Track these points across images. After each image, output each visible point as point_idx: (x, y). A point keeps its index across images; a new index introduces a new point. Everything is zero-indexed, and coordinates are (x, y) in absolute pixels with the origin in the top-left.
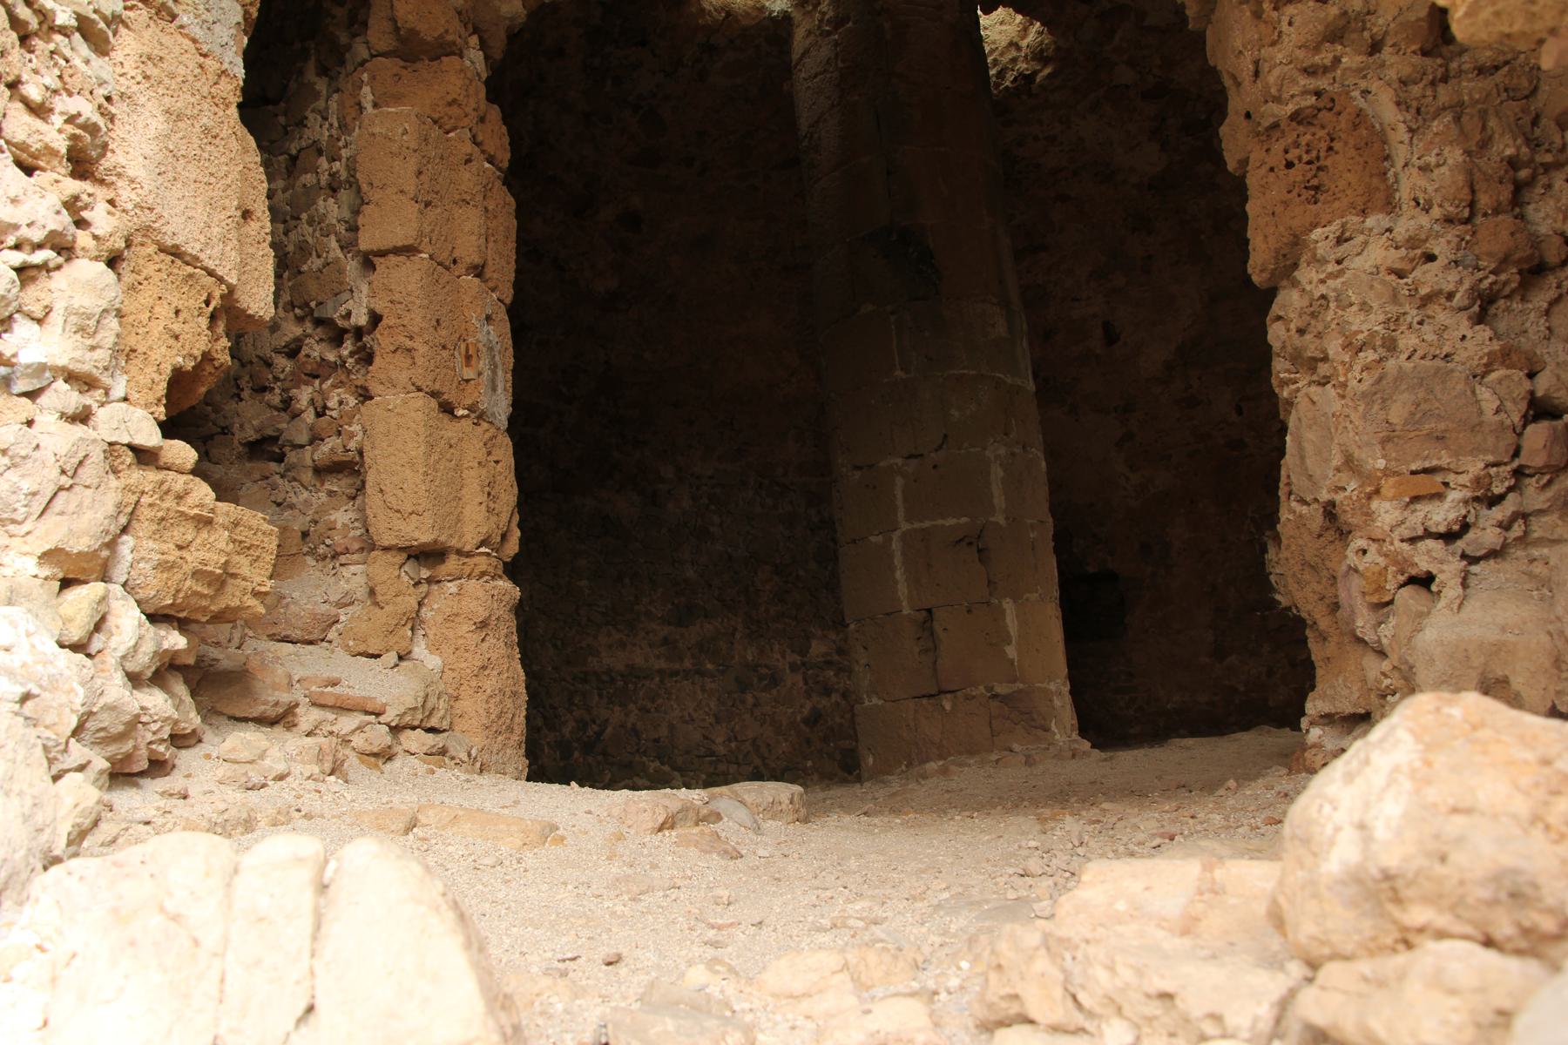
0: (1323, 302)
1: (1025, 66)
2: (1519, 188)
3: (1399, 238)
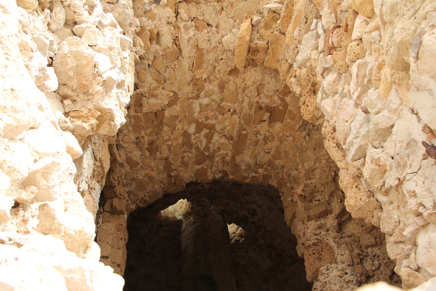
0: (325, 283)
1: (237, 238)
2: (361, 260)
3: (339, 269)
